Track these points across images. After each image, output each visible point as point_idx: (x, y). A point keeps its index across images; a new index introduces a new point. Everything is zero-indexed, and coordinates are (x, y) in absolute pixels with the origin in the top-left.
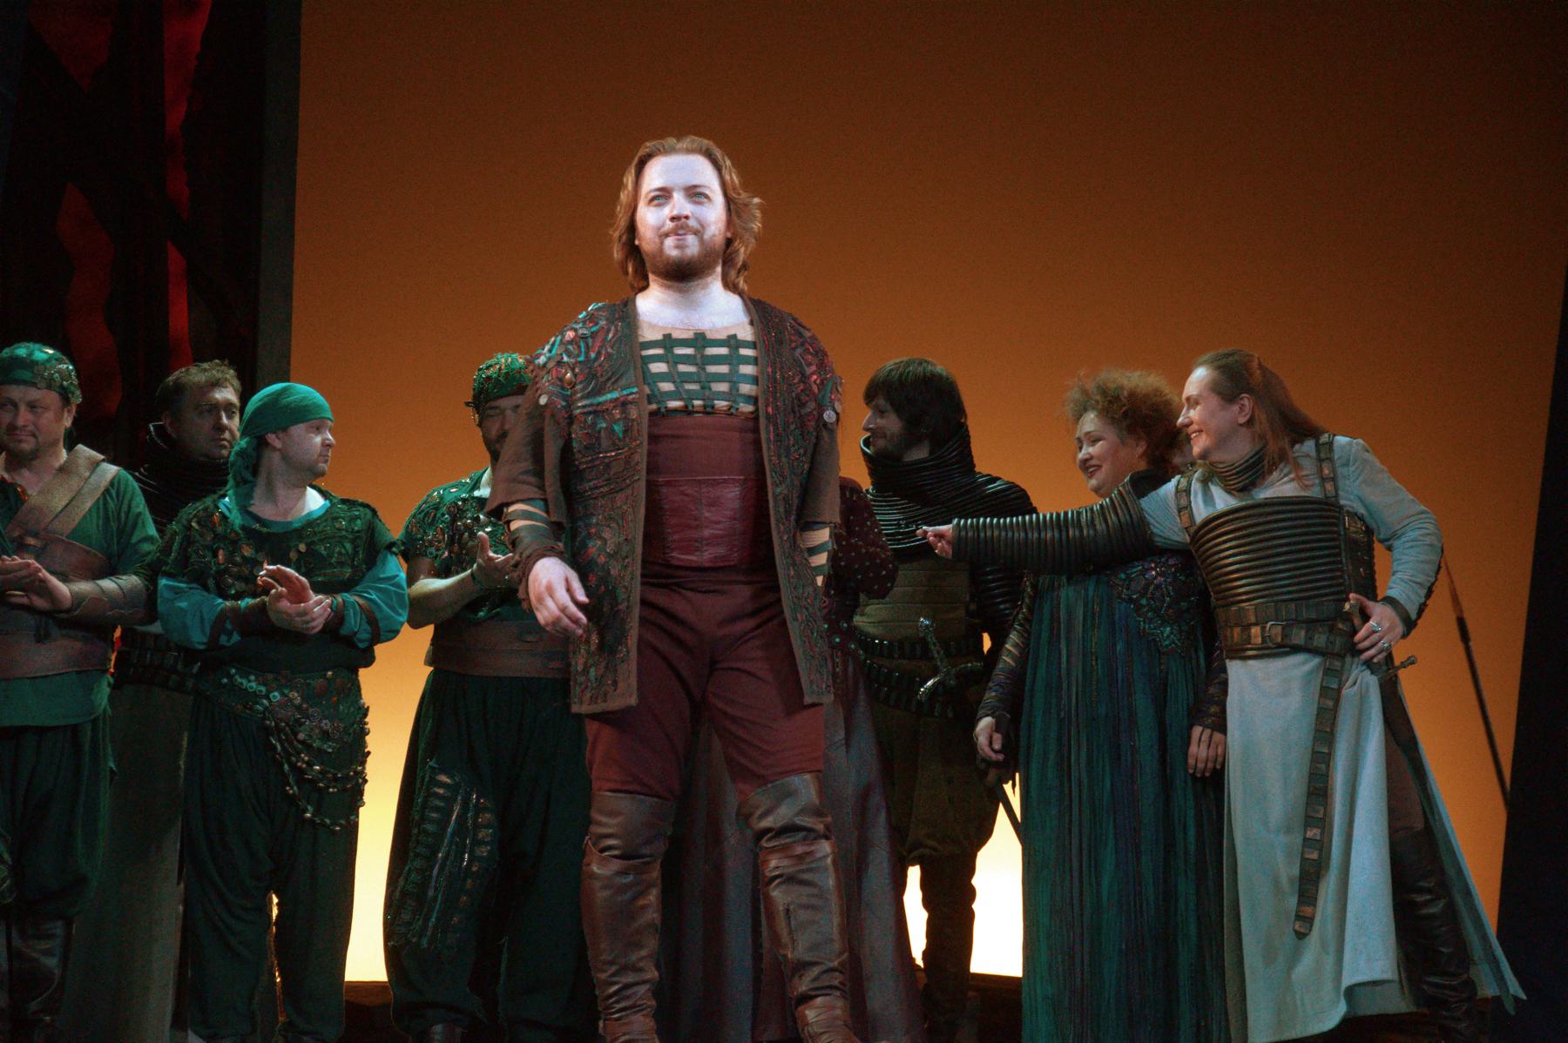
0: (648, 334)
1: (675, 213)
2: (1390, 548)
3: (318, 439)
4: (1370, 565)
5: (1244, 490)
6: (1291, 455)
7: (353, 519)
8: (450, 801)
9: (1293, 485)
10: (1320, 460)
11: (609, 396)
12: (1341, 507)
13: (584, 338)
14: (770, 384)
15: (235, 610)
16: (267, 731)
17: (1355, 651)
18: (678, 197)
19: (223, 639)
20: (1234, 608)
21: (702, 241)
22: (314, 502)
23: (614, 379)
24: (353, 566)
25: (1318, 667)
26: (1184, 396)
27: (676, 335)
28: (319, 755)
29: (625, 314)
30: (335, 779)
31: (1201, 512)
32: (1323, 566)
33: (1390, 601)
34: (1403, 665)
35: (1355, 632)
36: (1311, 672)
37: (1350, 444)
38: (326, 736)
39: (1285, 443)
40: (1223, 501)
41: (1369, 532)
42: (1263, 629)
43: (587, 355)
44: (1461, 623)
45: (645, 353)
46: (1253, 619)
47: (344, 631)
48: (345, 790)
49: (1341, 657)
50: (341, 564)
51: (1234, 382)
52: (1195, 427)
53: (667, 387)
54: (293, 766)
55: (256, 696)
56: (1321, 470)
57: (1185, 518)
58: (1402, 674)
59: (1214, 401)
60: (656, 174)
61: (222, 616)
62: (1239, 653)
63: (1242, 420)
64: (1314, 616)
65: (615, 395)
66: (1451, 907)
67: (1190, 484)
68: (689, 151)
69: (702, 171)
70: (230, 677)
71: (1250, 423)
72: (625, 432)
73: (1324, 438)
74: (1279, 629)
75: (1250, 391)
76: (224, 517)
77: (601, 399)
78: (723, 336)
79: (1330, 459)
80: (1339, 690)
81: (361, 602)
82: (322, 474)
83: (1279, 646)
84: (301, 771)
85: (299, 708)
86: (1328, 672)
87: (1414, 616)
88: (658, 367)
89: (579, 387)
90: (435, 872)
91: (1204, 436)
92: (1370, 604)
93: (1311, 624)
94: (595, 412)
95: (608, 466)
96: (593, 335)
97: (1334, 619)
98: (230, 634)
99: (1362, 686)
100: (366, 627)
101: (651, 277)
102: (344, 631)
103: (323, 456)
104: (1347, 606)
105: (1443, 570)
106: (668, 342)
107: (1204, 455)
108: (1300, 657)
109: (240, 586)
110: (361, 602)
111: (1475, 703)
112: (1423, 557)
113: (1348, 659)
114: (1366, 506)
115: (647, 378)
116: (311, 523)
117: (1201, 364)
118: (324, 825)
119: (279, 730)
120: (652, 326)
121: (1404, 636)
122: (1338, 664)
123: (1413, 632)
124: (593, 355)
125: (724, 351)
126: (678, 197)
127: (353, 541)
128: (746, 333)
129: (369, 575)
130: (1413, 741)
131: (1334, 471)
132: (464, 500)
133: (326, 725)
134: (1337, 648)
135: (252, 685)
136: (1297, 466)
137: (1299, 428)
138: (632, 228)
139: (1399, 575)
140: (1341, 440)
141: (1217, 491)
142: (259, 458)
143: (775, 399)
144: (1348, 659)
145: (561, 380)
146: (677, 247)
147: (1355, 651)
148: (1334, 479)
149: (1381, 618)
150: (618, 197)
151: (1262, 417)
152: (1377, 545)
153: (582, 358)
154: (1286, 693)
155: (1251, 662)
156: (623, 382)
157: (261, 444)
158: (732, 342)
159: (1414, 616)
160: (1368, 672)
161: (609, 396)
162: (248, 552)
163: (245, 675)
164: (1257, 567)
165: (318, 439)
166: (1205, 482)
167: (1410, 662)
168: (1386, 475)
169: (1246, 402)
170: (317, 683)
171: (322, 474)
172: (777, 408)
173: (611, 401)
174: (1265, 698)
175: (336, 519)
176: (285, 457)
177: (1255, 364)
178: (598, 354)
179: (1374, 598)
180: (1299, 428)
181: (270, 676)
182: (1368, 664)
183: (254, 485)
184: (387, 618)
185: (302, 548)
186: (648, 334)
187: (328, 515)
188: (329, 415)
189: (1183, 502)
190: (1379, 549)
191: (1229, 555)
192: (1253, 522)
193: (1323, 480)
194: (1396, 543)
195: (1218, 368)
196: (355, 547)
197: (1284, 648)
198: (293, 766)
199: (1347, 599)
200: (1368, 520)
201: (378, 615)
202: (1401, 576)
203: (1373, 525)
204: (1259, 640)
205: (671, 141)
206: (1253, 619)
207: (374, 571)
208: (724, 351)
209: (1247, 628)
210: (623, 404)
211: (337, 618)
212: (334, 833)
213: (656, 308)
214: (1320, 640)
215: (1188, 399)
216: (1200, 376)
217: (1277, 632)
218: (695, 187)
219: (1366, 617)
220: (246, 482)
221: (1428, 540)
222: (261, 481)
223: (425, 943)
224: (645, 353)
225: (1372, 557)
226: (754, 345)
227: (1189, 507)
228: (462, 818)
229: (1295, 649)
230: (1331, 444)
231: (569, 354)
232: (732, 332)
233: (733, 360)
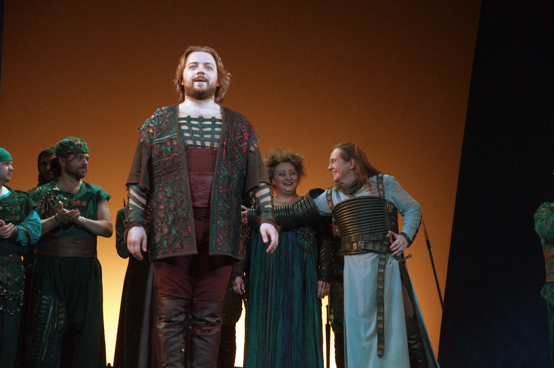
0: (182, 115)
1: (200, 71)
2: (403, 215)
3: (7, 168)
4: (396, 222)
5: (351, 194)
6: (367, 181)
8: (48, 306)
9: (369, 192)
10: (378, 183)
11: (166, 137)
12: (385, 200)
13: (158, 117)
14: (226, 135)
17: (390, 252)
20: (347, 236)
21: (208, 84)
23: (167, 131)
24: (20, 215)
25: (377, 257)
26: (331, 158)
27: (192, 117)
29: (175, 110)
31: (336, 202)
32: (379, 221)
33: (403, 234)
34: (407, 258)
35: (390, 245)
36: (374, 259)
37: (389, 178)
38: (8, 279)
39: (366, 177)
40: (344, 197)
41: (395, 209)
42: (357, 244)
43: (158, 122)
44: (428, 242)
45: (180, 122)
46: (354, 241)
47: (18, 240)
48: (15, 299)
49: (385, 254)
50: (16, 214)
51: (348, 154)
52: (334, 170)
53: (187, 135)
56: (379, 187)
57: (330, 204)
58: (406, 260)
59: (341, 161)
60: (193, 58)
62: (349, 252)
63: (351, 168)
64: (375, 239)
65: (168, 136)
66: (422, 345)
67: (331, 192)
68: (207, 52)
69: (210, 59)
71: (354, 169)
72: (172, 150)
73: (380, 175)
74: (363, 244)
75: (354, 158)
77: (163, 139)
78: (210, 117)
79: (382, 183)
80: (385, 266)
81: (24, 228)
83: (363, 250)
86: (381, 259)
87: (411, 240)
88: (185, 127)
89: (155, 134)
90: (45, 332)
91: (338, 173)
92: (395, 235)
93: (374, 242)
94: (161, 144)
95: (165, 164)
96: (161, 116)
97: (383, 240)
99: (393, 264)
100: (26, 238)
101: (186, 97)
102: (18, 240)
103: (9, 174)
104: (388, 235)
105: (422, 224)
106: (189, 119)
107: (337, 181)
108: (370, 254)
110: (24, 228)
111: (432, 270)
112: (414, 218)
113: (388, 254)
114: (395, 201)
115: (181, 132)
117: (338, 147)
118: (7, 312)
120: (183, 113)
121: (408, 247)
122: (384, 256)
123: (411, 245)
124: (160, 123)
125: (210, 123)
128: (219, 116)
129: (26, 219)
130: (410, 285)
131: (383, 187)
132: (50, 191)
133: (9, 275)
134: (383, 251)
136: (370, 185)
137: (371, 172)
138: (182, 78)
139: (406, 225)
140: (386, 176)
141: (341, 194)
144: (388, 254)
145: (149, 133)
146: (199, 86)
147: (390, 252)
148: (383, 190)
149: (400, 240)
151: (358, 167)
152: (399, 214)
153: (156, 124)
154: (365, 267)
155: (353, 256)
156: (171, 132)
158: (213, 120)
159: (411, 240)
160: (395, 260)
161: (166, 137)
164: (354, 222)
165: (7, 168)
166: (337, 191)
167: (409, 256)
168: (402, 189)
169: (353, 161)
171: (8, 181)
172: (227, 141)
173: (167, 139)
174: (358, 269)
175: (13, 198)
177: (356, 148)
178: (163, 122)
179: (398, 233)
180: (371, 172)
182: (395, 257)
184: (34, 234)
186: (182, 115)
187: (10, 197)
188: (11, 159)
189: (329, 199)
190: (399, 215)
191: (346, 217)
192: (355, 204)
193: (379, 190)
194: (405, 213)
195: (343, 149)
196: (21, 208)
197: (364, 251)
199: (388, 233)
200: (396, 206)
201: (30, 234)
202: (407, 225)
203: (397, 207)
204: (356, 248)
205: (199, 48)
206: (354, 241)
207: (29, 216)
208: (210, 123)
209: (352, 243)
210: (171, 140)
212: (11, 315)
213: (188, 108)
214: (377, 248)
215: (332, 160)
216: (336, 152)
217: (362, 245)
218: (208, 63)
219: (394, 240)
221: (417, 212)
224: (180, 122)
225: (397, 218)
226: (221, 121)
227: (331, 200)
228: (53, 311)
229: (369, 251)
230: (382, 177)
231: (152, 123)
232: (213, 116)
233: (213, 126)
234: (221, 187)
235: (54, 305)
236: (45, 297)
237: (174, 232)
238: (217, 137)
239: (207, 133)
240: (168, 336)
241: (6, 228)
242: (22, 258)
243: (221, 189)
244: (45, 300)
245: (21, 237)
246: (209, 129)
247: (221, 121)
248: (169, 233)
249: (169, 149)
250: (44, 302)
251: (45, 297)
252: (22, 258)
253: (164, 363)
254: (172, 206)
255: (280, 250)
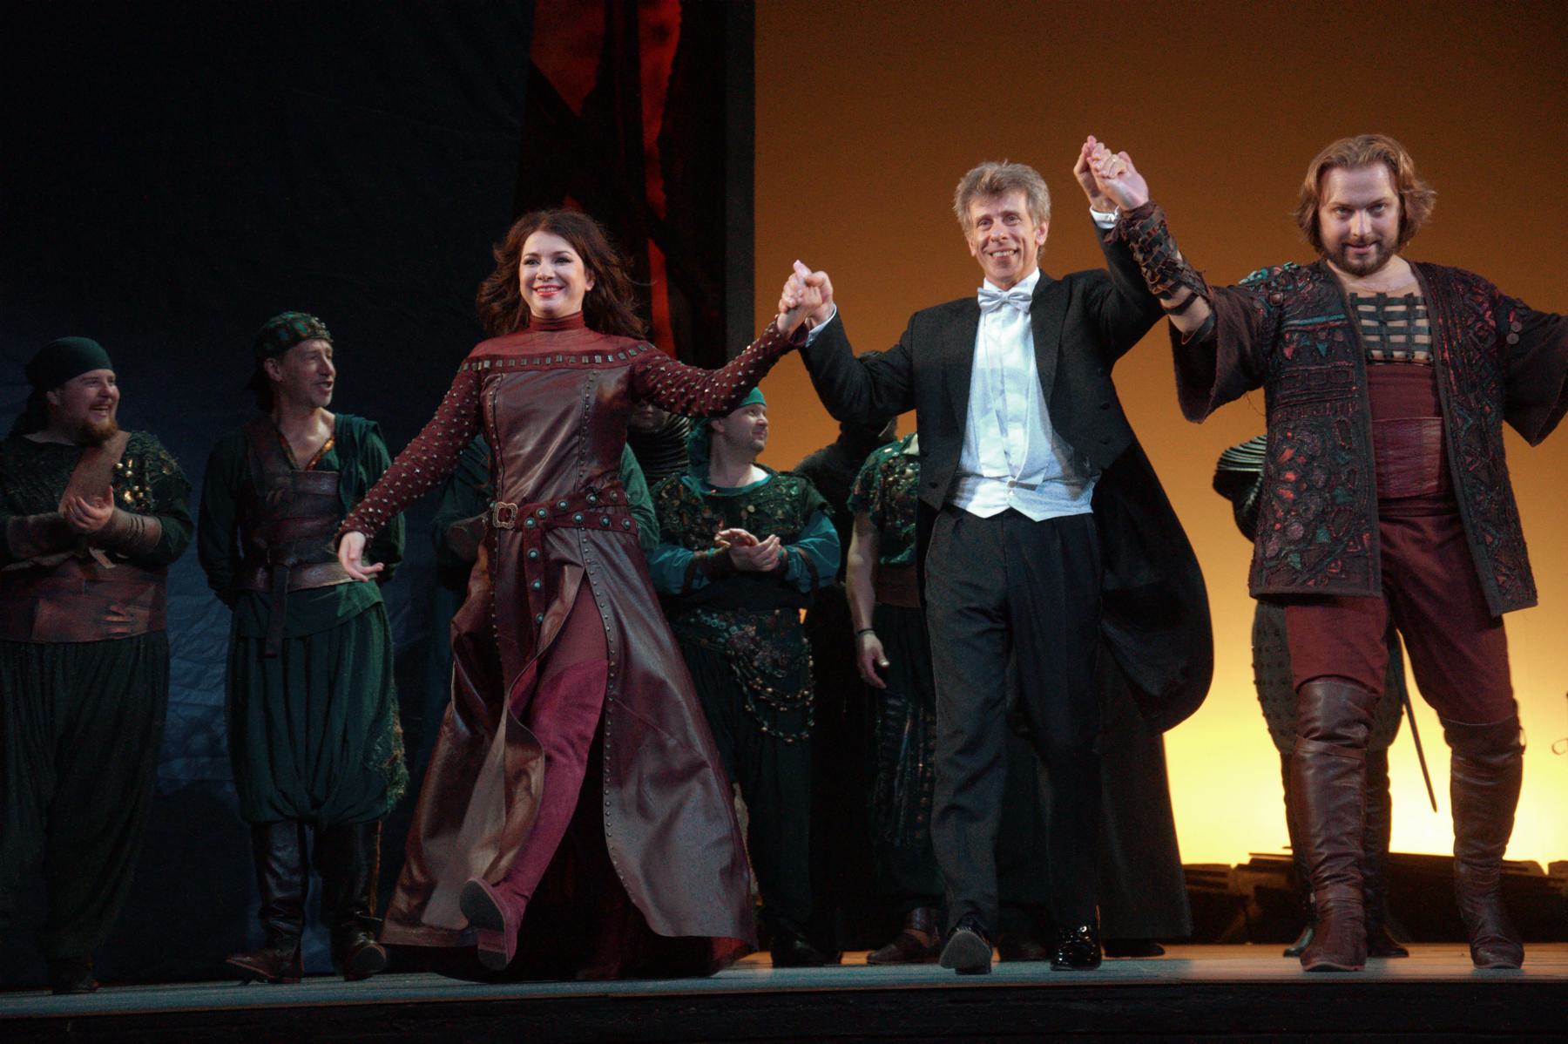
7: (791, 486)
15: (704, 560)
16: (729, 659)
18: (998, 221)
19: (695, 583)
22: (758, 475)
28: (770, 679)
30: (786, 700)
38: (776, 664)
47: (789, 577)
54: (750, 688)
55: (717, 631)
61: (694, 564)
70: (696, 616)
72: (1329, 350)
76: (687, 489)
78: (1401, 295)
82: (760, 449)
84: (756, 693)
85: (753, 639)
98: (701, 579)
102: (789, 577)
109: (702, 542)
116: (756, 488)
119: (738, 658)
126: (998, 221)
127: (791, 504)
133: (777, 654)
135: (715, 621)
142: (710, 441)
143: (1449, 340)
150: (506, 231)
157: (709, 431)
158: (1409, 300)
162: (708, 514)
163: (709, 614)
170: (767, 619)
171: (760, 449)
176: (728, 438)
181: (729, 614)
183: (709, 464)
185: (751, 508)
187: (772, 483)
198: (750, 688)
208: (1402, 308)
211: (784, 563)
220: (700, 463)
222: (713, 460)
223: (897, 842)
224: (1389, 309)
228: (912, 732)
233: (1409, 316)
234: (1469, 459)
235: (915, 717)
236: (892, 702)
237: (1323, 537)
238: (1423, 339)
239: (1398, 331)
240: (1331, 772)
241: (765, 547)
242: (803, 612)
243: (1471, 463)
244: (894, 708)
245: (796, 570)
246: (1401, 323)
247: (602, 475)
248: (1308, 539)
249: (1322, 348)
250: (1365, 322)
251: (892, 702)
252: (803, 612)
253: (1316, 836)
254: (1319, 477)
255: (1546, 322)
